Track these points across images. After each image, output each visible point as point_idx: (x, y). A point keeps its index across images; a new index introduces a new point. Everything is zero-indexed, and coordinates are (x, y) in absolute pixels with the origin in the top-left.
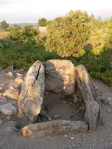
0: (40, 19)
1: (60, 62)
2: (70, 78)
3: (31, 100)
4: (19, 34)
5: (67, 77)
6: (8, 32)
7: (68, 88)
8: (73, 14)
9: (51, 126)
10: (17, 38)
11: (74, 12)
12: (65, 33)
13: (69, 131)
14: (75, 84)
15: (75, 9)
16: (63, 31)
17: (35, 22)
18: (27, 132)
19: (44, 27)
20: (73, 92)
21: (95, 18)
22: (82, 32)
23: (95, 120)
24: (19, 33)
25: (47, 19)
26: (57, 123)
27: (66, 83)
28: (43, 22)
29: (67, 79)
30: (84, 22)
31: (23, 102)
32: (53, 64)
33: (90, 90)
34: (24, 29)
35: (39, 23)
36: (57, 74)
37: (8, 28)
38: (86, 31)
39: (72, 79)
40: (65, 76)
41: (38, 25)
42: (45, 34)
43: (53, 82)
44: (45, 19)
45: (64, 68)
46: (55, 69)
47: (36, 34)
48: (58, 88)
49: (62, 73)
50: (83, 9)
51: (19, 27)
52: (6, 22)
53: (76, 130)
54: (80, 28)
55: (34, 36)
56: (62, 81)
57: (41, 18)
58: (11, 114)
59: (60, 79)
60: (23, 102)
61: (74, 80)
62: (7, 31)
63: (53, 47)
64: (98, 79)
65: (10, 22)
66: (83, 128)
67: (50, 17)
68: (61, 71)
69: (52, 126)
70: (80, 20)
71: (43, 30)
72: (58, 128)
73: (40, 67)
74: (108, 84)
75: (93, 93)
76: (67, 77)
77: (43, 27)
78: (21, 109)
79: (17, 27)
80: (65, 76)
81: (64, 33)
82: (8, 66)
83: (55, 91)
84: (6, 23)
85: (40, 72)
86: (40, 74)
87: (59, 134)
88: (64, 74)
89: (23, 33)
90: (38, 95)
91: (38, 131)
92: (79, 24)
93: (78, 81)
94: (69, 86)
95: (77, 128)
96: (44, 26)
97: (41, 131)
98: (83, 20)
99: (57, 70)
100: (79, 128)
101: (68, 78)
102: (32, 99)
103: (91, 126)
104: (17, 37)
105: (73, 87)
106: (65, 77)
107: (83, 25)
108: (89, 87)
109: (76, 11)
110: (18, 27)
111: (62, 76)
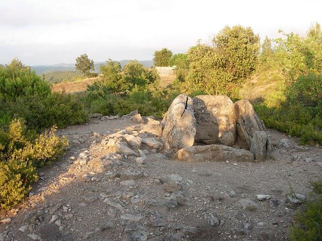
0: (158, 51)
1: (213, 99)
2: (228, 121)
3: (181, 131)
4: (118, 80)
5: (224, 119)
6: (91, 78)
7: (226, 136)
8: (229, 31)
9: (209, 150)
10: (114, 88)
11: (231, 29)
12: (218, 59)
13: (231, 157)
14: (235, 129)
15: (232, 24)
16: (216, 55)
17: (145, 57)
18: (183, 154)
19: (166, 68)
20: (233, 141)
21: (271, 48)
22: (245, 58)
23: (262, 147)
24: (118, 78)
25: (172, 52)
26: (217, 147)
27: (222, 127)
28: (164, 58)
29: (223, 122)
30: (246, 43)
31: (172, 134)
32: (202, 101)
33: (256, 123)
34: (127, 71)
35: (156, 60)
36: (209, 114)
37: (91, 71)
38: (249, 57)
39: (231, 122)
40: (220, 118)
41: (152, 65)
42: (168, 82)
43: (203, 127)
44: (170, 52)
45: (217, 105)
46: (205, 107)
47: (152, 79)
48: (211, 136)
49: (215, 113)
50: (245, 25)
51: (120, 67)
52: (89, 58)
53: (239, 156)
54: (241, 52)
55: (149, 84)
56: (217, 125)
57: (160, 49)
58: (156, 146)
59: (213, 122)
60: (172, 134)
61: (234, 123)
62: (89, 75)
63: (200, 82)
64: (270, 128)
65: (98, 58)
66: (247, 156)
67: (180, 46)
68: (215, 111)
69: (212, 150)
70: (241, 39)
71: (166, 73)
72: (218, 153)
73: (187, 99)
74: (285, 132)
75: (257, 121)
76: (224, 119)
77: (163, 68)
78: (169, 142)
79: (113, 68)
80: (220, 118)
81: (216, 58)
82: (130, 111)
83: (205, 141)
84: (88, 61)
85: (188, 103)
86: (189, 106)
87: (220, 160)
88: (218, 114)
89: (127, 79)
90: (191, 124)
91: (195, 154)
92: (239, 46)
93: (240, 121)
94: (226, 132)
95: (240, 155)
96: (166, 65)
97: (199, 155)
98: (245, 40)
99: (209, 108)
100: (243, 155)
101: (225, 121)
102: (182, 129)
103: (257, 155)
104: (115, 85)
105: (232, 134)
106: (221, 120)
107: (246, 48)
108: (254, 121)
109: (234, 27)
110: (116, 66)
111: (215, 118)
